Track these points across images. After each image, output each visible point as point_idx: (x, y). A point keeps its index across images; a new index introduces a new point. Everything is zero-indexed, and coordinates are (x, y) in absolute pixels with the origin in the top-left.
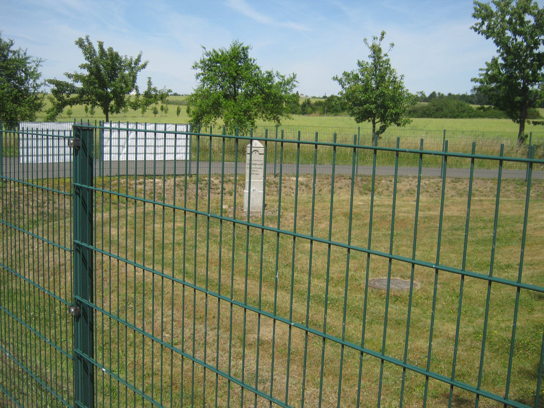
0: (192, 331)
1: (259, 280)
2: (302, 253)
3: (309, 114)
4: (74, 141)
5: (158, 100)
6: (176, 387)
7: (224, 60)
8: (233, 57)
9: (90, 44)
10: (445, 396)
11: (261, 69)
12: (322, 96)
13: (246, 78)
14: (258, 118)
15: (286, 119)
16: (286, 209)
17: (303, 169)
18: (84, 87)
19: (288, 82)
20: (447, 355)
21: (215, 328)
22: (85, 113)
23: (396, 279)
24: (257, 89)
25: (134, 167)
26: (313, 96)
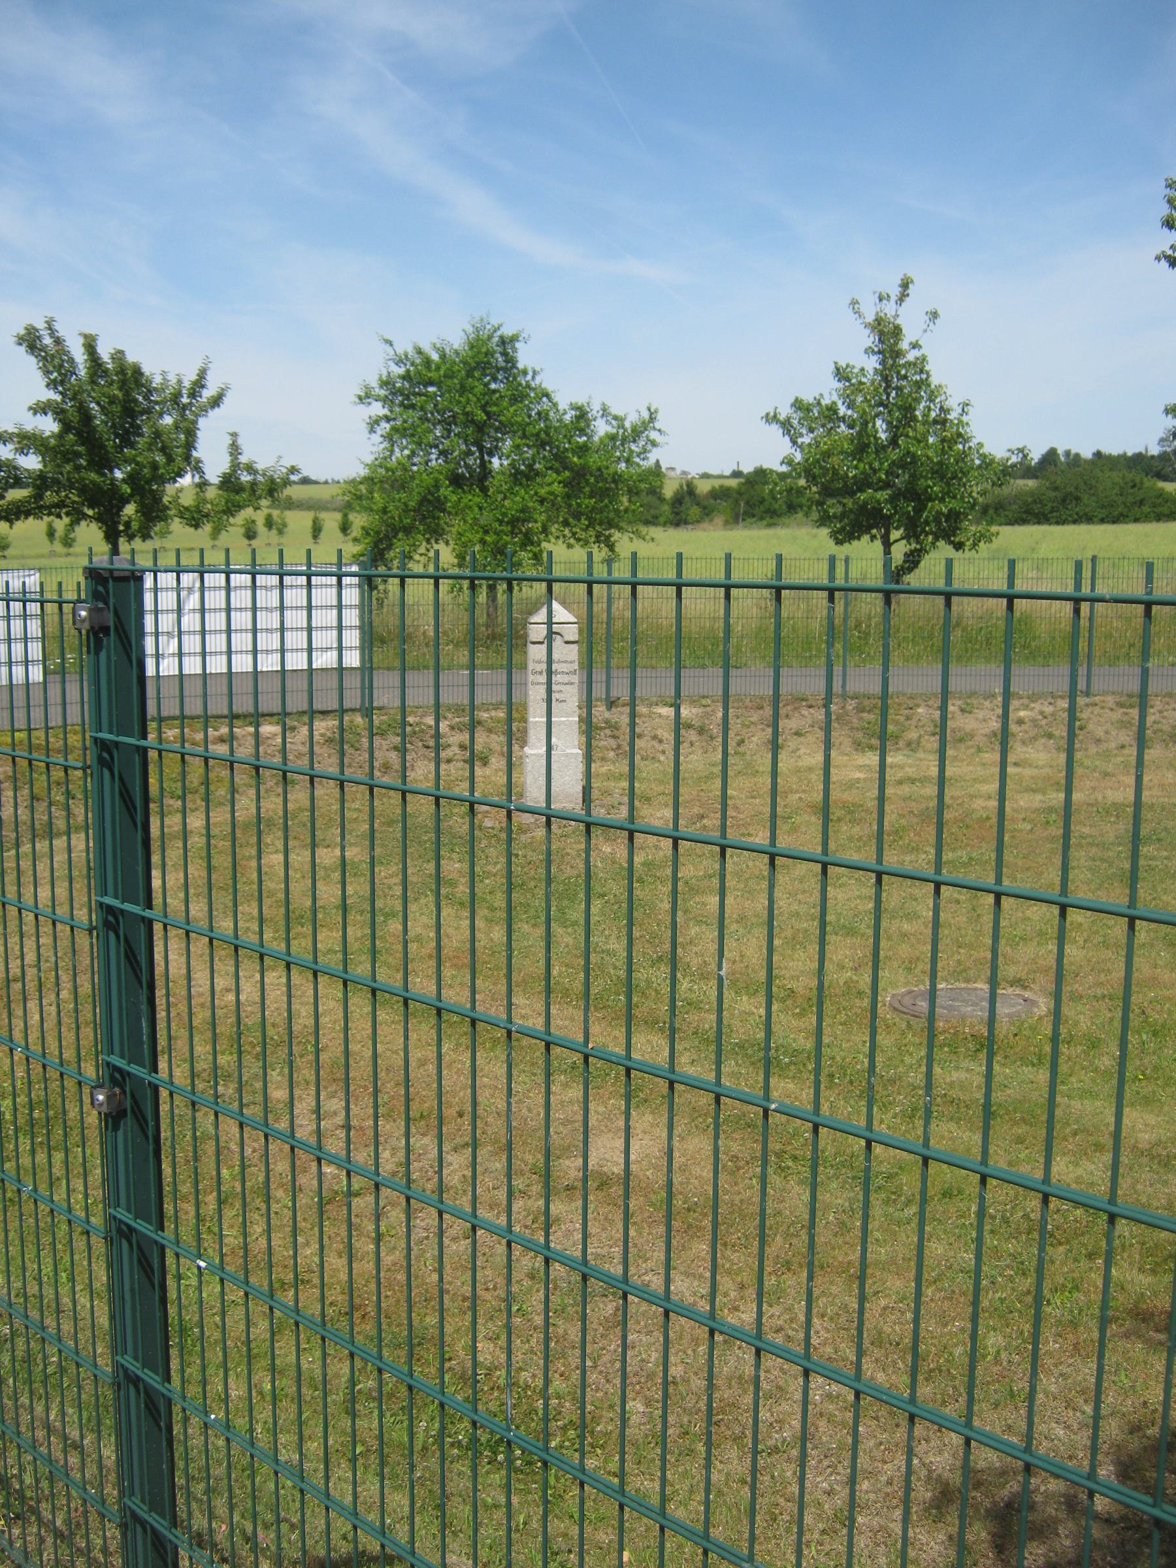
0: (401, 1154)
1: (582, 1003)
2: (699, 923)
3: (692, 523)
4: (90, 611)
5: (260, 497)
6: (363, 1316)
7: (450, 375)
8: (473, 364)
9: (58, 341)
10: (1138, 1315)
11: (557, 398)
12: (728, 473)
13: (512, 425)
14: (553, 540)
15: (631, 539)
16: (648, 799)
17: (693, 682)
18: (45, 466)
19: (636, 433)
20: (1138, 1200)
21: (467, 1144)
22: (48, 542)
23: (976, 989)
24: (544, 457)
25: (177, 693)
26: (701, 472)
